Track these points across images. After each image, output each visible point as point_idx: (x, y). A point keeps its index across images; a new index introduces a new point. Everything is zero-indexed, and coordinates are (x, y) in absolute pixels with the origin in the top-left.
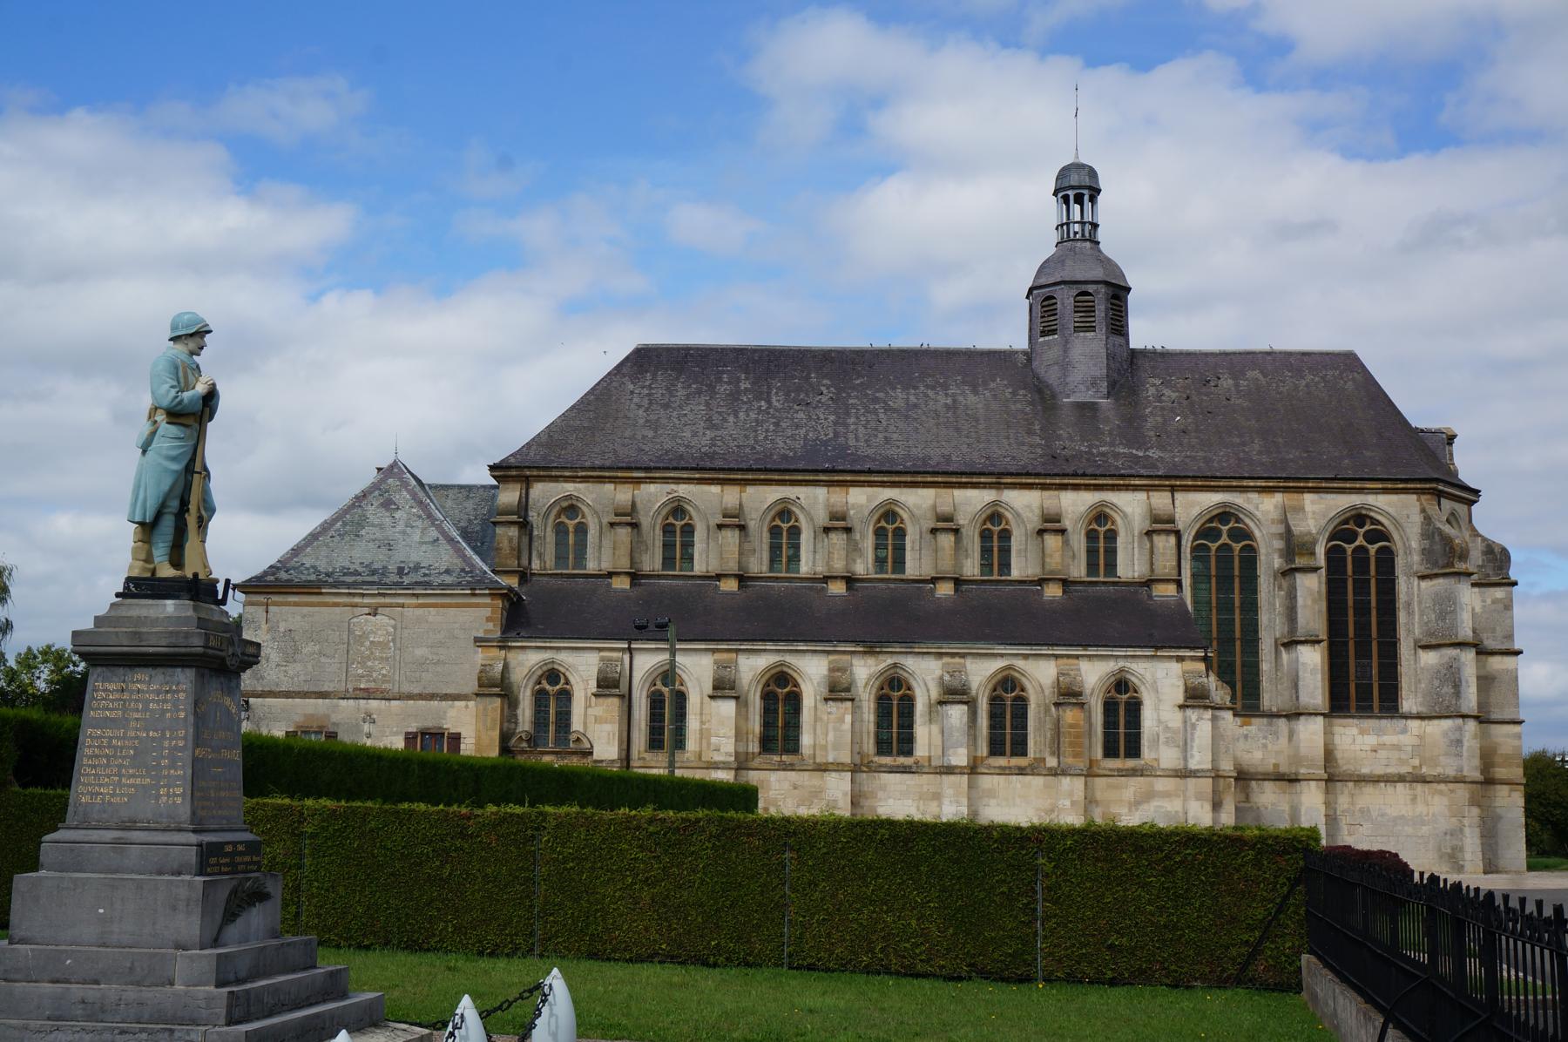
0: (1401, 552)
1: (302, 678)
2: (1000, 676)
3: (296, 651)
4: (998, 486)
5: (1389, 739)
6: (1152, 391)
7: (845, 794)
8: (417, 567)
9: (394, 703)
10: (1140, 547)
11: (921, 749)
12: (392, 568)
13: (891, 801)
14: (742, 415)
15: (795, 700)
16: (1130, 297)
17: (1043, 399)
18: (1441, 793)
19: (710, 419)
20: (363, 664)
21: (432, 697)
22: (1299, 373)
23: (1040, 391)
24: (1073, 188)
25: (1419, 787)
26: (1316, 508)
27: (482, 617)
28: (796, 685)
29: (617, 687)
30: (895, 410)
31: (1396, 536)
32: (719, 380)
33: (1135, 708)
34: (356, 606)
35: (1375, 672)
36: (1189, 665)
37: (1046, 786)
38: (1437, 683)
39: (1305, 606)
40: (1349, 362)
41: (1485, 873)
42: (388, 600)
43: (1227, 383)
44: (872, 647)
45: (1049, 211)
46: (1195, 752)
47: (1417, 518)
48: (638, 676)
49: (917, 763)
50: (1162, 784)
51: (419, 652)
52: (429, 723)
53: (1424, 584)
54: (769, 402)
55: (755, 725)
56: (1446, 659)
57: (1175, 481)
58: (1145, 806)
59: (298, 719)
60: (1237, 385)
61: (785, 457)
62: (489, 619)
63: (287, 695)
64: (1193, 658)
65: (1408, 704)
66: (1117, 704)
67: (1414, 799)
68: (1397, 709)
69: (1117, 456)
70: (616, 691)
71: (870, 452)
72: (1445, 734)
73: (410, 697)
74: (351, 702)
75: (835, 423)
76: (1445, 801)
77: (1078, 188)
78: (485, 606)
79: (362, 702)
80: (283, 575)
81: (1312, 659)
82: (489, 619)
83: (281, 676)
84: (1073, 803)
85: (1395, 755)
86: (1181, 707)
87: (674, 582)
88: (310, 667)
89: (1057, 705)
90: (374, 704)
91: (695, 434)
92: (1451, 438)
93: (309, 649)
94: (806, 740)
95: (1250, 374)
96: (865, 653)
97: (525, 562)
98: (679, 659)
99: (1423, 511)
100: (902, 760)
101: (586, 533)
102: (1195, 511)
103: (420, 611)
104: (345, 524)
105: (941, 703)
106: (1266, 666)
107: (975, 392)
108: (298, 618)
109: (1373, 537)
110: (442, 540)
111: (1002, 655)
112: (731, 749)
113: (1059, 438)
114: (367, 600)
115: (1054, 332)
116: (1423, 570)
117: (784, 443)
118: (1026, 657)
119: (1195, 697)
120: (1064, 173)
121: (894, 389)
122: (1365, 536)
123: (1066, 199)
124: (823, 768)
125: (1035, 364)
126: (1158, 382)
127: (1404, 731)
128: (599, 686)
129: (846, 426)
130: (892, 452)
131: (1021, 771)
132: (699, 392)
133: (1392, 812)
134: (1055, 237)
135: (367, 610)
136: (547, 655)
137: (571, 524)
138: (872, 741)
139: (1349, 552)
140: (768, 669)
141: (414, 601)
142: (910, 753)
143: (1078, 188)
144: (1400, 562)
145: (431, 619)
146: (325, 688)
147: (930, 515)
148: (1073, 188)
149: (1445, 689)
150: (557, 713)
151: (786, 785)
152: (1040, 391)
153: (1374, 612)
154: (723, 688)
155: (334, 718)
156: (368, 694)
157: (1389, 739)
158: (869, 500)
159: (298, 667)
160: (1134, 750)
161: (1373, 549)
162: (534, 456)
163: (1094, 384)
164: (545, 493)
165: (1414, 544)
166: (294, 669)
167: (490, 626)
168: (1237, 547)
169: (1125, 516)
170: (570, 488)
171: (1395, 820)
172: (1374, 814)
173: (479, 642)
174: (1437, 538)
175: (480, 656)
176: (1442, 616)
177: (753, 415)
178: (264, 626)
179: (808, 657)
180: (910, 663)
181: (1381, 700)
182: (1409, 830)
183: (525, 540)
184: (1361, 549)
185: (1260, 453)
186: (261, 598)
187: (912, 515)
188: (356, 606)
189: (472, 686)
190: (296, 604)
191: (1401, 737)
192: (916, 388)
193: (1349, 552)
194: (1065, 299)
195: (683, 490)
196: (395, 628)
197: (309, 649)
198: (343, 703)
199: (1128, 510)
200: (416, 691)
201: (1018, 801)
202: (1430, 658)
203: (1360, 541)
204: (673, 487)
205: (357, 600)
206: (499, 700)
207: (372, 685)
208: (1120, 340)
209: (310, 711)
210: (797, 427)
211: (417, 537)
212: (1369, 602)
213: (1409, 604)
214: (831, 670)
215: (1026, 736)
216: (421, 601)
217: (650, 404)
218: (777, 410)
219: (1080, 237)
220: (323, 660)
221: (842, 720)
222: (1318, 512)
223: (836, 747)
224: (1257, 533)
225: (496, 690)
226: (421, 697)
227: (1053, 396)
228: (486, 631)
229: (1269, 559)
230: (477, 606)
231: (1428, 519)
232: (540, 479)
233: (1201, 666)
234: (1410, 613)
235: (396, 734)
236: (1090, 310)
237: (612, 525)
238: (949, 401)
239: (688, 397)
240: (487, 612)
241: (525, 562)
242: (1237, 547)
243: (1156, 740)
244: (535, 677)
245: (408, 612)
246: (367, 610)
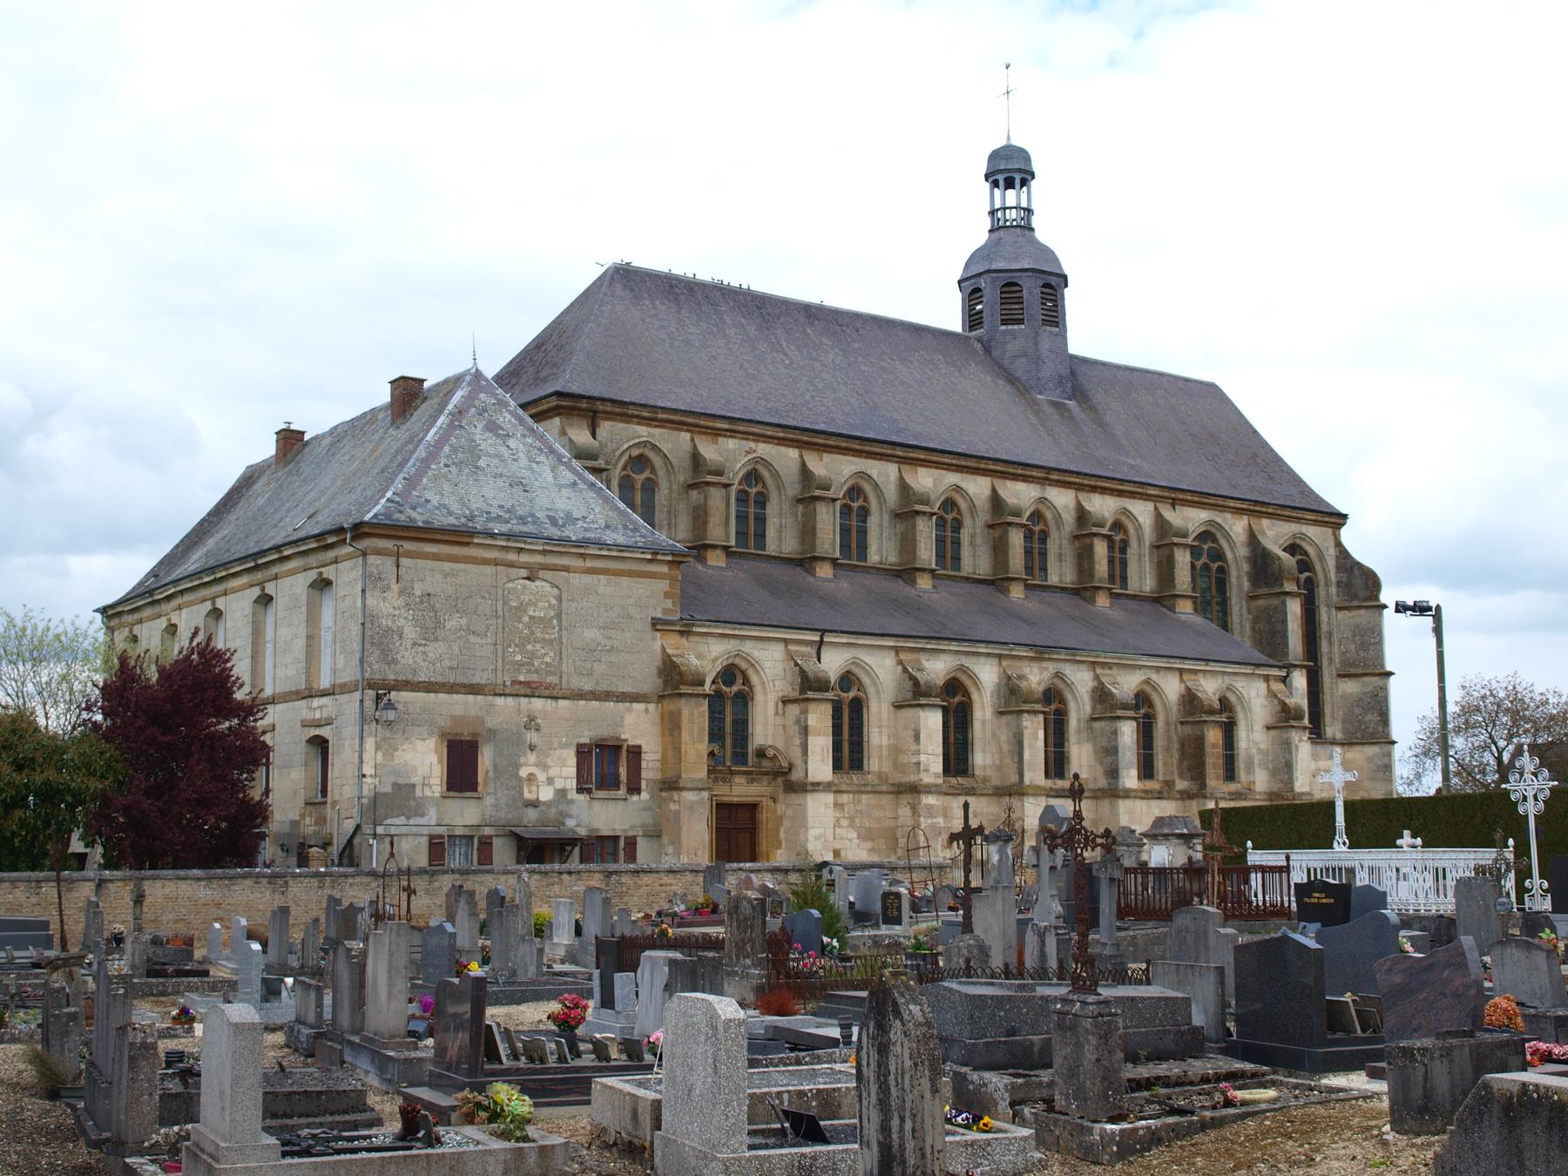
0: (1322, 583)
1: (447, 663)
3: (438, 625)
9: (562, 703)
16: (1068, 293)
20: (521, 647)
21: (606, 696)
24: (1001, 171)
27: (650, 595)
29: (702, 684)
31: (1318, 568)
34: (511, 565)
40: (1211, 392)
42: (550, 560)
44: (1041, 652)
45: (979, 196)
51: (591, 634)
52: (604, 732)
53: (1341, 614)
56: (1370, 688)
62: (667, 595)
63: (429, 687)
70: (699, 690)
72: (1370, 760)
74: (510, 700)
77: (1009, 170)
78: (661, 576)
79: (524, 701)
82: (667, 595)
83: (419, 659)
88: (456, 650)
90: (538, 703)
93: (454, 622)
96: (1032, 659)
103: (588, 579)
108: (439, 577)
114: (524, 558)
115: (1021, 321)
118: (1158, 669)
120: (995, 156)
123: (995, 184)
134: (987, 223)
135: (524, 573)
136: (731, 646)
137: (640, 478)
141: (579, 563)
143: (1009, 170)
144: (1321, 592)
145: (601, 589)
146: (476, 680)
148: (1001, 171)
149: (1369, 717)
150: (735, 722)
156: (531, 690)
159: (441, 647)
165: (1333, 576)
166: (435, 650)
167: (669, 604)
173: (656, 624)
175: (657, 642)
176: (1364, 646)
178: (395, 587)
179: (982, 660)
186: (388, 544)
188: (511, 565)
190: (436, 557)
196: (560, 599)
197: (454, 622)
198: (500, 701)
200: (588, 688)
202: (1350, 687)
204: (752, 445)
205: (512, 557)
207: (534, 678)
209: (459, 711)
213: (1330, 634)
216: (589, 564)
219: (1012, 230)
220: (472, 638)
228: (665, 611)
230: (653, 575)
232: (610, 416)
234: (1331, 643)
235: (566, 746)
240: (664, 585)
243: (1250, 769)
245: (576, 579)
246: (524, 573)
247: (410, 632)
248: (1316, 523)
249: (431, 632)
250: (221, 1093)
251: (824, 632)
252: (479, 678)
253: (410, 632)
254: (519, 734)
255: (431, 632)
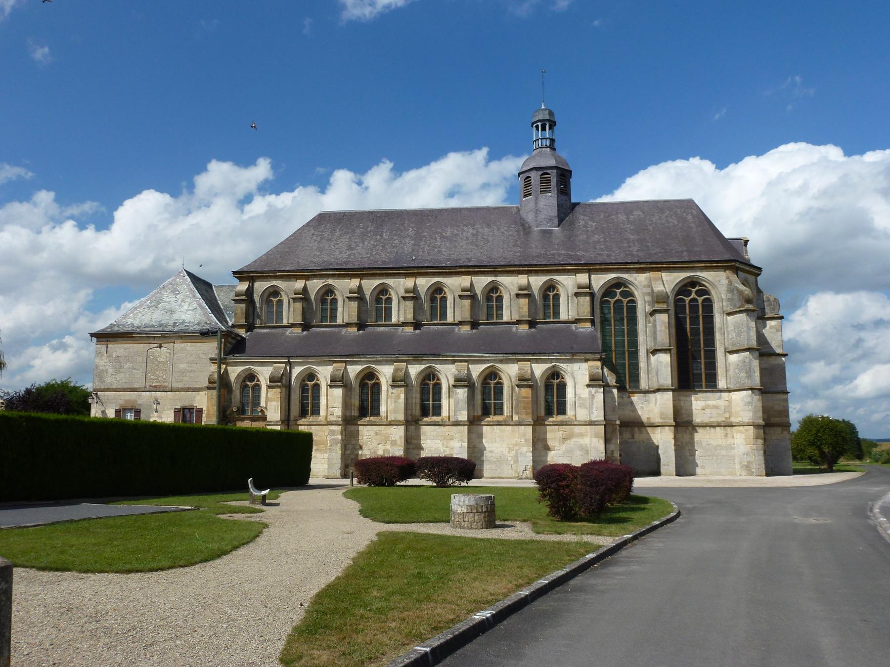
2: (550, 372)
3: (121, 367)
4: (495, 273)
5: (710, 403)
6: (582, 223)
7: (401, 437)
8: (184, 322)
10: (572, 303)
11: (445, 412)
12: (171, 323)
13: (428, 441)
14: (366, 243)
15: (377, 386)
17: (524, 229)
18: (741, 432)
19: (350, 246)
22: (662, 211)
23: (523, 225)
25: (729, 429)
26: (668, 278)
27: (211, 348)
28: (378, 379)
30: (445, 237)
32: (358, 227)
33: (562, 387)
35: (703, 366)
36: (591, 363)
37: (513, 431)
38: (737, 371)
39: (661, 331)
40: (690, 204)
41: (767, 475)
43: (622, 217)
44: (417, 358)
46: (594, 410)
47: (725, 282)
48: (294, 376)
49: (442, 420)
50: (577, 429)
51: (183, 366)
52: (186, 404)
53: (729, 318)
54: (381, 236)
55: (356, 402)
57: (591, 268)
58: (569, 441)
59: (121, 402)
60: (628, 218)
61: (384, 262)
63: (116, 390)
64: (594, 360)
65: (722, 384)
66: (552, 385)
67: (726, 435)
68: (715, 386)
69: (559, 255)
71: (429, 258)
72: (742, 399)
73: (178, 390)
75: (414, 245)
76: (743, 436)
80: (116, 329)
81: (664, 360)
84: (526, 440)
85: (714, 411)
86: (588, 386)
87: (324, 329)
89: (518, 386)
91: (341, 253)
92: (746, 242)
94: (383, 408)
95: (635, 213)
97: (251, 320)
98: (229, 368)
99: (728, 278)
100: (435, 418)
101: (446, 301)
102: (602, 283)
104: (152, 302)
105: (454, 386)
106: (642, 365)
107: (489, 226)
109: (701, 293)
110: (198, 309)
111: (488, 360)
112: (340, 414)
113: (531, 248)
115: (530, 194)
116: (729, 310)
117: (383, 257)
118: (501, 361)
119: (595, 381)
121: (446, 227)
122: (696, 292)
124: (390, 424)
125: (522, 212)
126: (586, 218)
127: (720, 398)
128: (590, 380)
129: (419, 246)
130: (440, 257)
131: (499, 424)
132: (347, 233)
133: (714, 443)
135: (156, 345)
138: (418, 407)
139: (687, 302)
140: (422, 371)
142: (439, 414)
144: (716, 307)
147: (459, 289)
151: (372, 433)
152: (523, 225)
153: (702, 334)
154: (335, 382)
155: (140, 401)
156: (156, 389)
157: (710, 403)
158: (427, 283)
159: (122, 375)
160: (562, 410)
161: (700, 300)
162: (246, 269)
163: (550, 220)
164: (260, 287)
168: (625, 301)
169: (564, 286)
170: (274, 283)
171: (716, 448)
172: (704, 444)
173: (212, 360)
174: (735, 292)
177: (372, 242)
180: (257, 369)
181: (706, 381)
182: (724, 452)
183: (251, 309)
184: (694, 300)
185: (638, 251)
187: (450, 289)
189: (206, 384)
191: (718, 401)
192: (458, 226)
193: (687, 302)
194: (535, 177)
195: (330, 281)
199: (565, 283)
201: (498, 439)
203: (693, 295)
206: (279, 390)
208: (564, 197)
209: (127, 398)
210: (394, 247)
211: (186, 307)
212: (699, 328)
214: (520, 369)
215: (502, 404)
217: (322, 239)
218: (385, 240)
220: (134, 371)
221: (398, 397)
222: (669, 281)
223: (395, 411)
224: (636, 293)
225: (465, 383)
226: (183, 390)
227: (530, 227)
229: (643, 307)
231: (730, 283)
233: (599, 363)
236: (548, 182)
237: (460, 296)
238: (475, 232)
239: (341, 235)
241: (251, 320)
242: (625, 301)
244: (241, 379)
247: (110, 371)
248: (707, 268)
249: (117, 371)
250: (507, 520)
251: (289, 358)
252: (136, 385)
253: (110, 371)
254: (151, 406)
255: (117, 371)
